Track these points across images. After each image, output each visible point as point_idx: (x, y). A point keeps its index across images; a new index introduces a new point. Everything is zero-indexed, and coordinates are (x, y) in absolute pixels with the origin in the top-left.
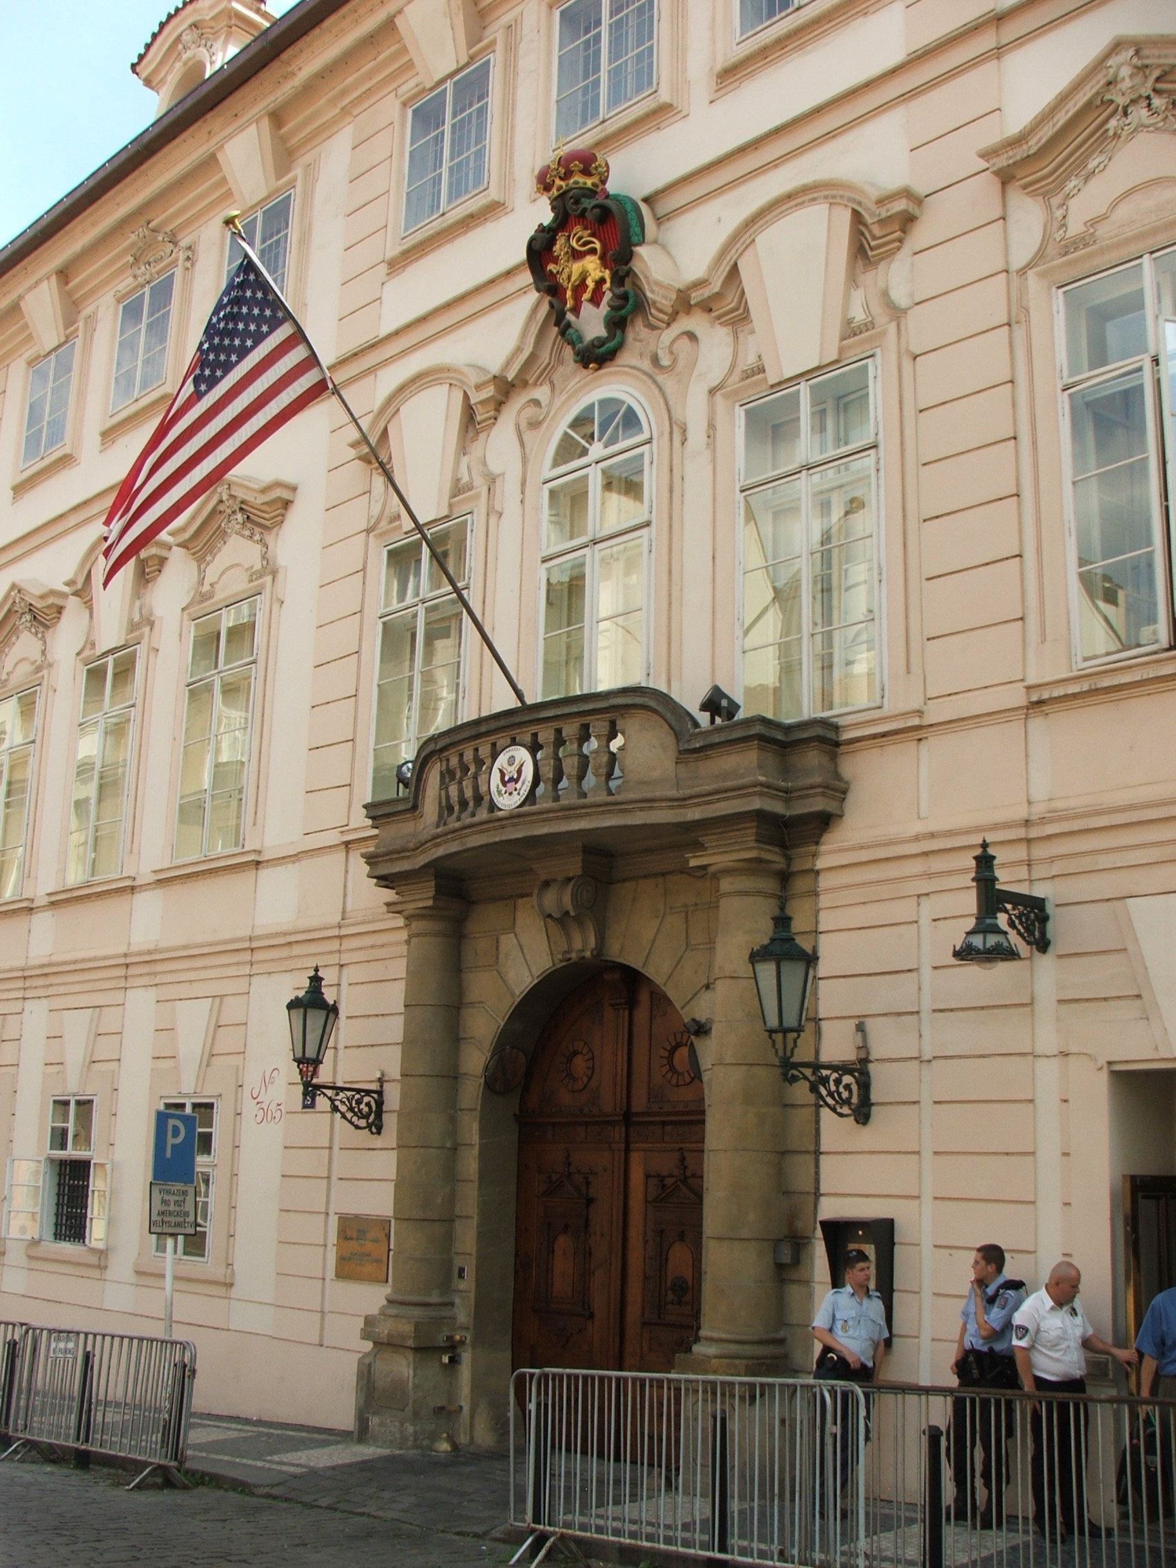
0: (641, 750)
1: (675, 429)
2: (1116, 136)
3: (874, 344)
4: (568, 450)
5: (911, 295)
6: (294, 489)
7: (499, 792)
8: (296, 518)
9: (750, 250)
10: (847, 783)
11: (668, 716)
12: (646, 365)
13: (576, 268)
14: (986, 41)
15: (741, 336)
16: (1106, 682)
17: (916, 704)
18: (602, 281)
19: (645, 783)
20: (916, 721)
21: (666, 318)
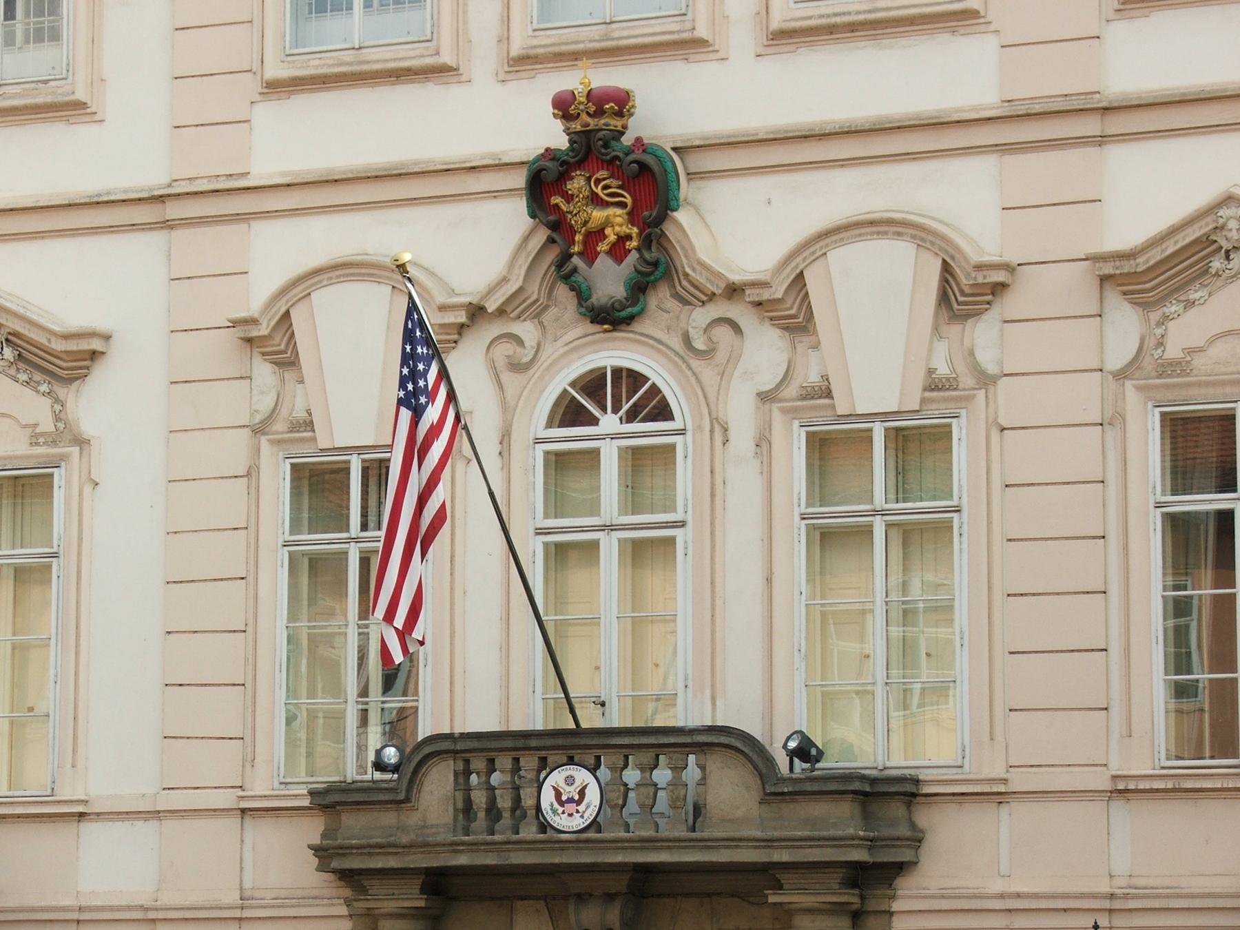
0: (729, 791)
1: (717, 429)
2: (1217, 275)
3: (959, 405)
4: (570, 413)
5: (1000, 363)
6: (107, 338)
7: (555, 812)
8: (102, 378)
9: (819, 263)
10: (922, 831)
11: (755, 757)
12: (676, 342)
13: (598, 215)
14: (1090, 126)
15: (800, 347)
16: (1189, 784)
17: (999, 772)
18: (623, 239)
19: (730, 821)
20: (1002, 789)
21: (705, 298)
